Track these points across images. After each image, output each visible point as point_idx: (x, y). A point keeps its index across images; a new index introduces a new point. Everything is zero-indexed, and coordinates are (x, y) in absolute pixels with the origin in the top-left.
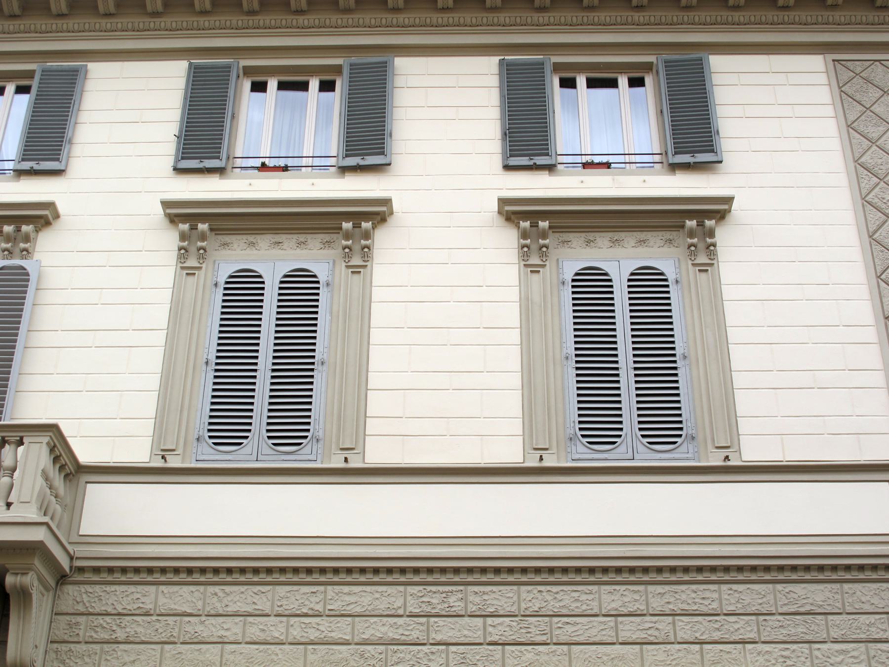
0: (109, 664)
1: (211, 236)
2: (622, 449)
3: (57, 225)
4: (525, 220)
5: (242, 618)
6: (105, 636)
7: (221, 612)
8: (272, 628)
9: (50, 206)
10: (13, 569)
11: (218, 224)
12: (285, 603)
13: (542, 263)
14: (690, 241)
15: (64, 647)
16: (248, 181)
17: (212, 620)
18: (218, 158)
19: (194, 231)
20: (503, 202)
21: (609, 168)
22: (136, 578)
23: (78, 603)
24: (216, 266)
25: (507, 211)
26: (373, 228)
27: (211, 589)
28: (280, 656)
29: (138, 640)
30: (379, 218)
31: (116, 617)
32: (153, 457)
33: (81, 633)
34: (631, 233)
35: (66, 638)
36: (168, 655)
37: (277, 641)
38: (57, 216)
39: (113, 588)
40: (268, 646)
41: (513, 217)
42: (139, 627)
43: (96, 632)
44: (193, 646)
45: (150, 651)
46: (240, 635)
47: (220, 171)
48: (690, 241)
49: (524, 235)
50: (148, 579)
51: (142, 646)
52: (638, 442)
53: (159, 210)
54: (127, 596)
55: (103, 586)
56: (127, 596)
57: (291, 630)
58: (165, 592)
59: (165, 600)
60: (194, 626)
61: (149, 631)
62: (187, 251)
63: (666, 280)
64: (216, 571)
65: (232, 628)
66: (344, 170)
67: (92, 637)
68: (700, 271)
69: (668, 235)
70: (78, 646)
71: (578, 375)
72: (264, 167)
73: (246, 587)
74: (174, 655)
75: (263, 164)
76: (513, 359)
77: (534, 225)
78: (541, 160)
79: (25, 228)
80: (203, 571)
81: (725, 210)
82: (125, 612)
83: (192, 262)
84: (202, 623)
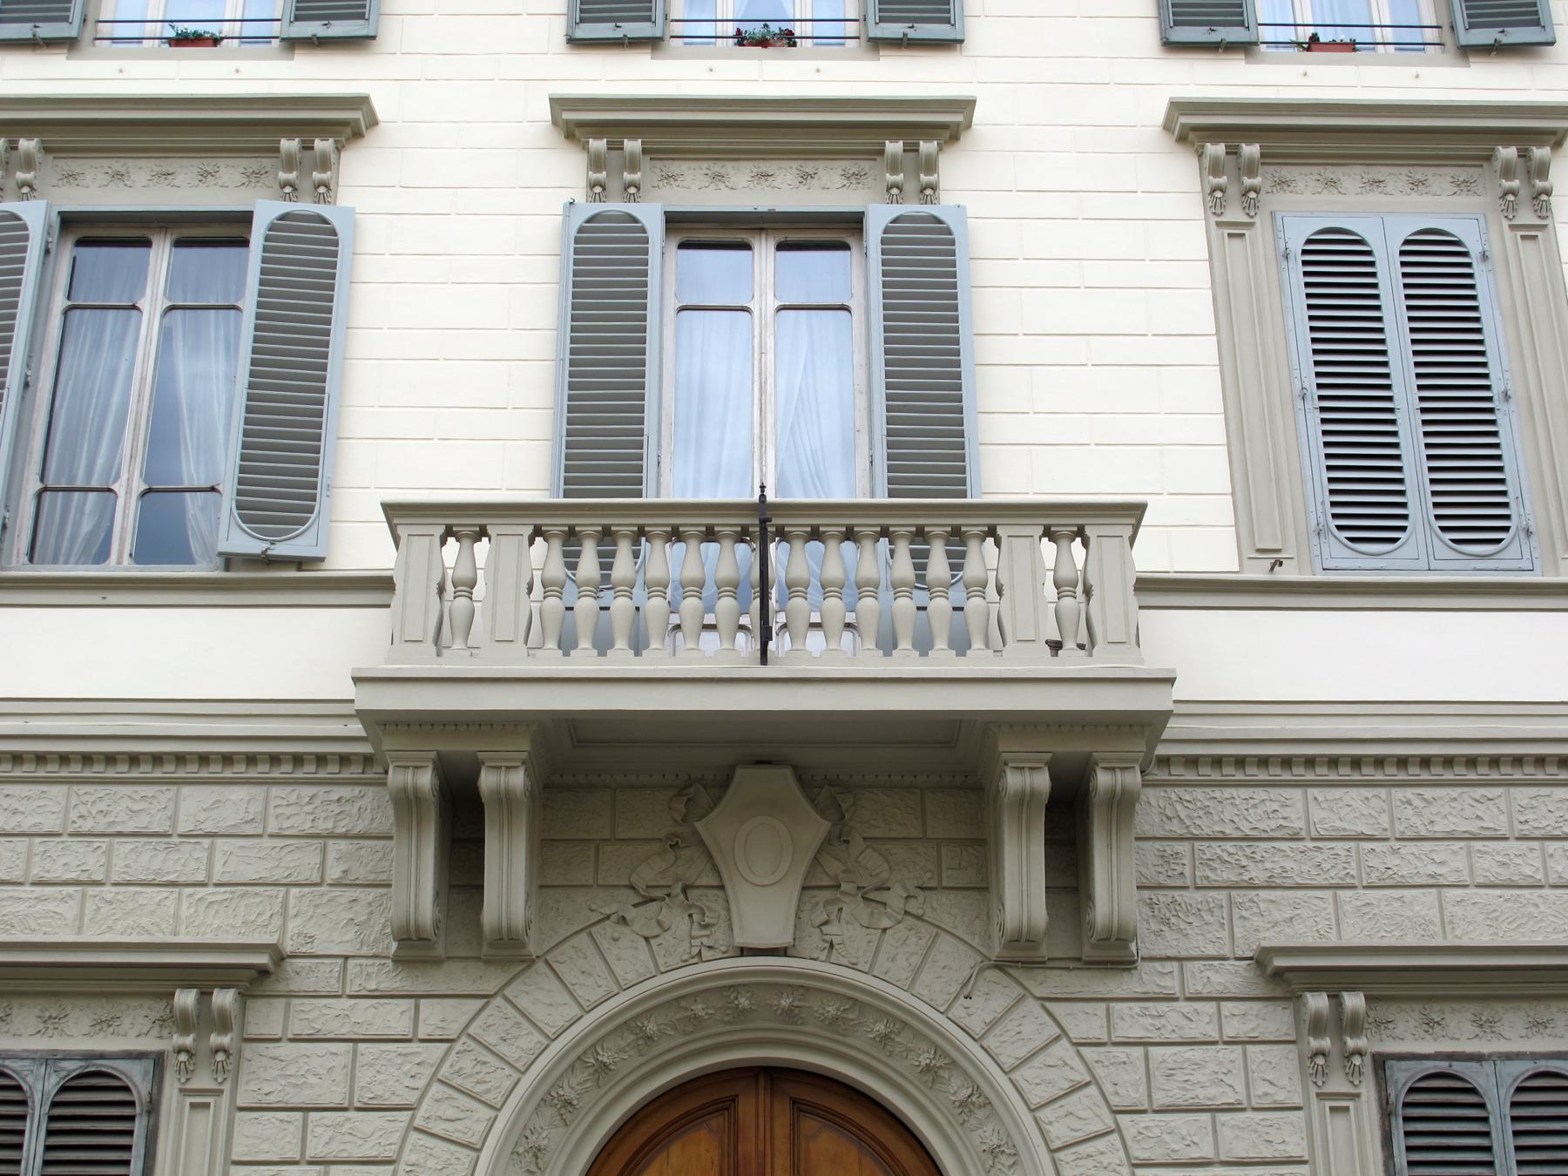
0: (1247, 923)
1: (645, 161)
2: (1514, 551)
3: (371, 137)
4: (598, 137)
5: (1462, 844)
6: (1230, 876)
7: (1424, 833)
8: (1518, 860)
9: (361, 102)
10: (1104, 760)
11: (56, 139)
12: (1532, 817)
13: (1248, 220)
14: (890, 178)
15: (1163, 897)
16: (1414, 70)
17: (1411, 847)
18: (648, 19)
19: (308, 153)
20: (559, 104)
21: (1354, 50)
22: (1263, 776)
23: (1169, 819)
24: (1279, 222)
25: (567, 122)
26: (338, 150)
27: (1399, 794)
28: (1542, 908)
29: (1289, 882)
30: (348, 131)
31: (1244, 844)
32: (1247, 563)
33: (1187, 871)
34: (92, 162)
35: (1162, 880)
36: (1347, 907)
37: (1529, 881)
38: (373, 122)
39: (1228, 792)
40: (1518, 892)
41: (577, 132)
42: (1288, 861)
43: (1213, 869)
44: (1387, 892)
45: (1316, 902)
46: (1466, 872)
47: (69, 44)
48: (890, 178)
49: (596, 163)
50: (1261, 777)
51: (1300, 893)
52: (1435, 539)
53: (545, 112)
54: (1255, 806)
55: (1208, 790)
56: (1255, 806)
57: (1551, 863)
58: (1320, 799)
59: (1323, 814)
60: (1381, 859)
61: (1305, 868)
62: (295, 189)
63: (1465, 254)
64: (1402, 762)
65: (1450, 861)
66: (293, 44)
67: (1207, 878)
68: (1523, 237)
69: (852, 166)
70: (1185, 893)
71: (1425, 422)
72: (1313, 43)
73: (1459, 790)
74: (1358, 909)
75: (1314, 39)
76: (1205, 388)
77: (615, 147)
78: (339, 29)
79: (320, 144)
80: (1379, 762)
81: (958, 124)
82: (1255, 834)
83: (1235, 214)
84: (1395, 852)
